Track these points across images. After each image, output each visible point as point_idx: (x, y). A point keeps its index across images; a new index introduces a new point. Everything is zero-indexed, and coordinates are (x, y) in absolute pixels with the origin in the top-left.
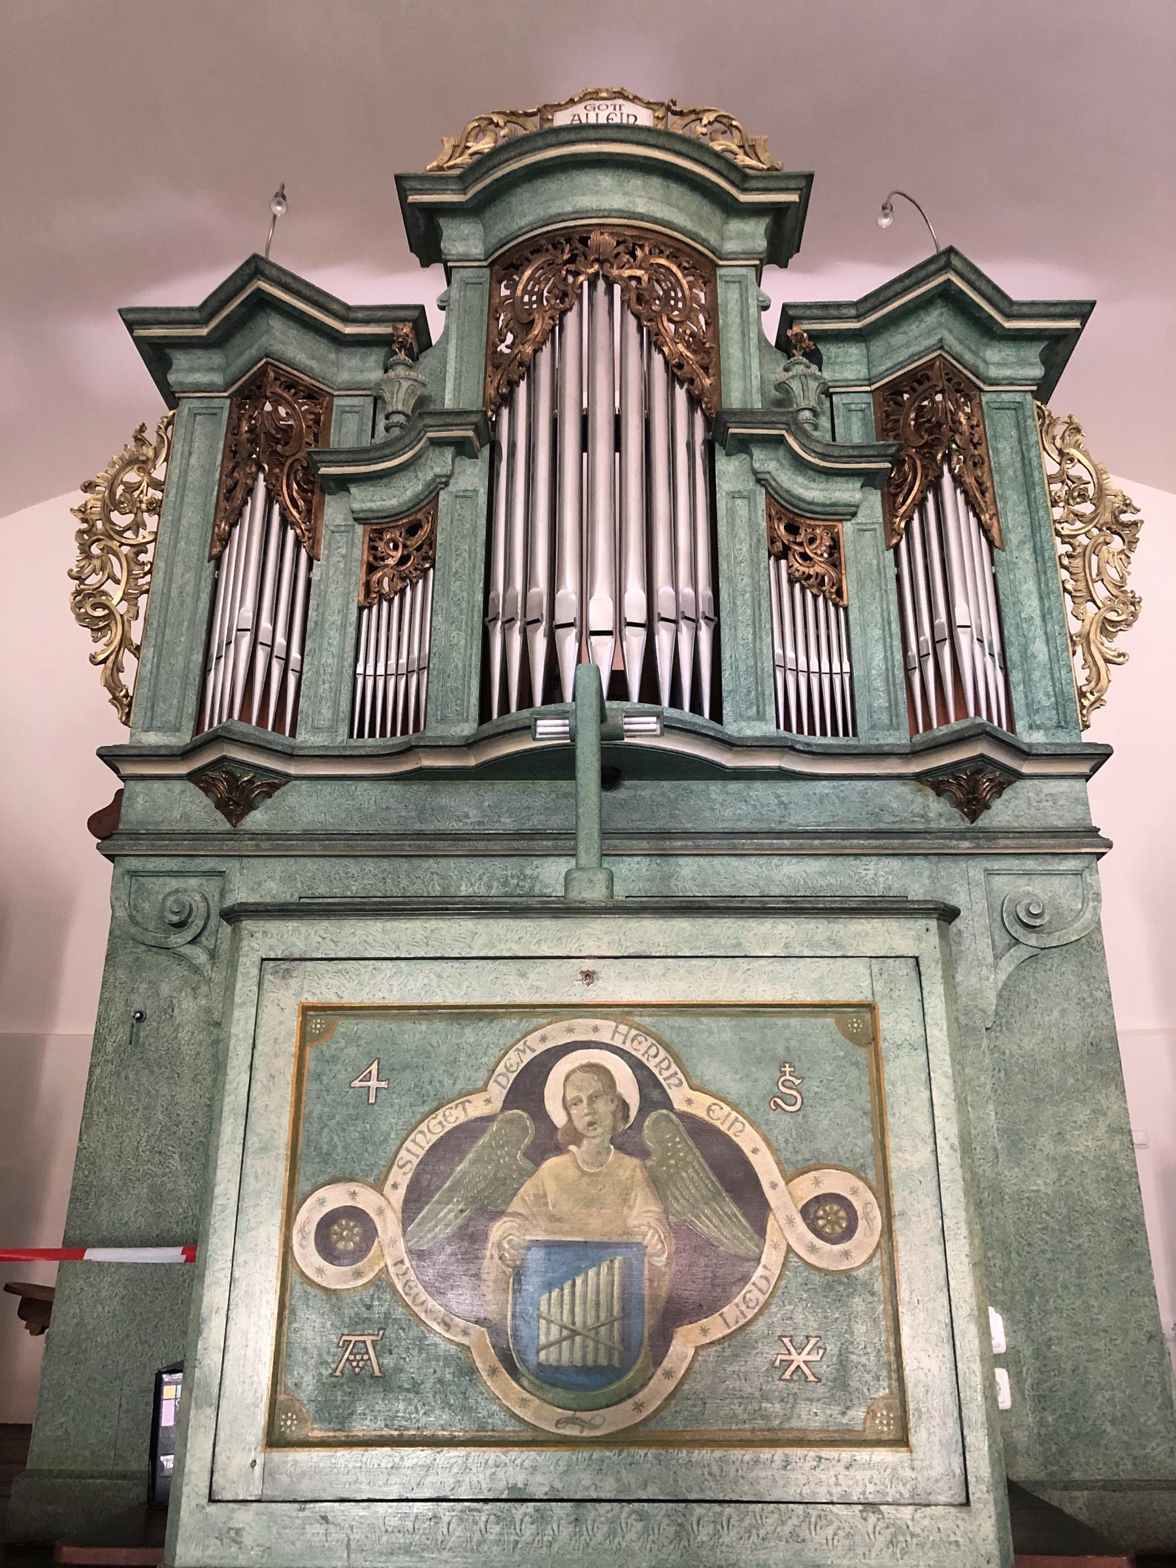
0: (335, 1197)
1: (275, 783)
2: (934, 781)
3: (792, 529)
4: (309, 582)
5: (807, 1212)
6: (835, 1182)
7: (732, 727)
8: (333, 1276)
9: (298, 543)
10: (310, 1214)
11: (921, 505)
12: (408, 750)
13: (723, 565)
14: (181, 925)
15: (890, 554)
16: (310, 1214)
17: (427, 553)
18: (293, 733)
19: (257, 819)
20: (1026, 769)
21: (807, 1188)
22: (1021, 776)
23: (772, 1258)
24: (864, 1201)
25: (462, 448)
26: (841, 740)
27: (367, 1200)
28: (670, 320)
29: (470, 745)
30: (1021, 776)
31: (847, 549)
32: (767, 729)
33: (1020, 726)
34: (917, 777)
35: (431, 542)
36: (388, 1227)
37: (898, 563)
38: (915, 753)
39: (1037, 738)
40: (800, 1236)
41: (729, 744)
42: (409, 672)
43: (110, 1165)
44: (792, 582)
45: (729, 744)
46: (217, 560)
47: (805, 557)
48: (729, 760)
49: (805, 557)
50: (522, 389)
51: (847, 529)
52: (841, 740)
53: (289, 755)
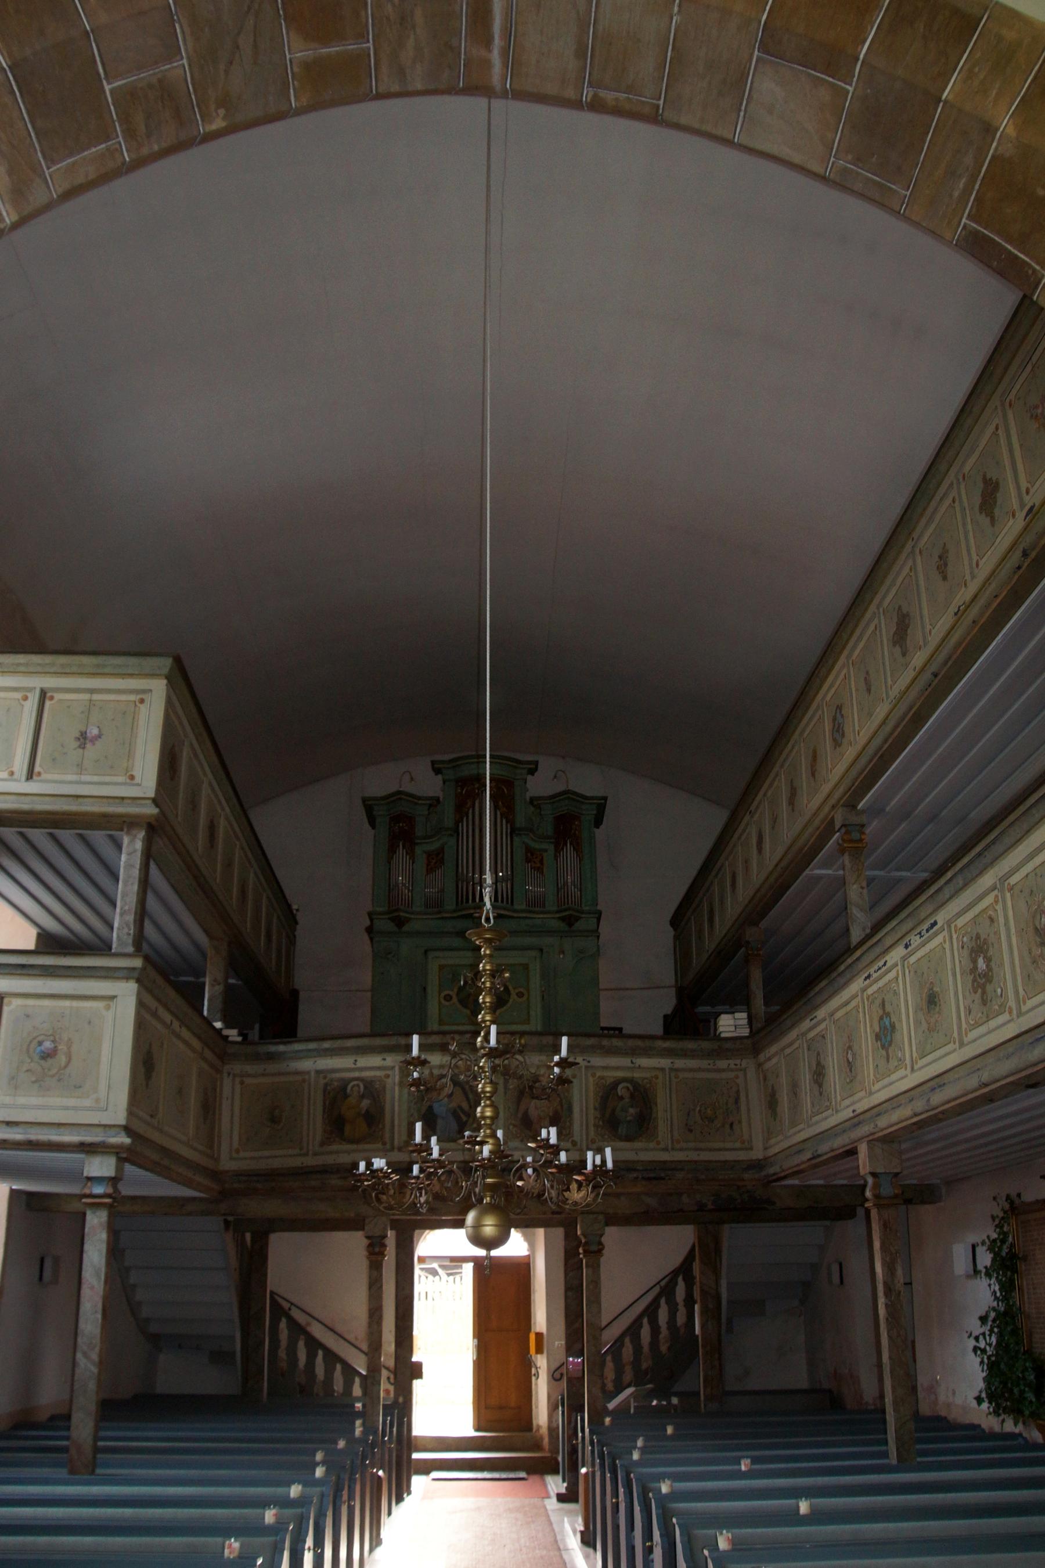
0: (446, 993)
1: (408, 920)
2: (562, 919)
3: (532, 854)
4: (413, 869)
5: (517, 994)
6: (522, 990)
7: (516, 907)
8: (447, 1003)
9: (410, 859)
10: (443, 995)
11: (563, 849)
12: (439, 912)
13: (514, 865)
14: (390, 953)
15: (555, 861)
16: (443, 995)
17: (442, 862)
18: (412, 908)
19: (406, 928)
20: (583, 916)
21: (517, 991)
22: (581, 918)
23: (511, 1000)
24: (525, 992)
25: (451, 835)
26: (542, 909)
27: (451, 993)
28: (484, 1102)
29: (455, 911)
30: (581, 918)
31: (545, 859)
32: (524, 907)
33: (583, 905)
34: (559, 918)
35: (443, 858)
36: (454, 997)
37: (557, 864)
38: (558, 912)
39: (587, 908)
40: (516, 997)
41: (515, 911)
42: (438, 892)
43: (493, 944)
44: (531, 869)
45: (515, 911)
46: (390, 863)
47: (534, 862)
48: (515, 915)
49: (534, 862)
50: (465, 819)
51: (545, 855)
52: (542, 909)
53: (412, 913)
